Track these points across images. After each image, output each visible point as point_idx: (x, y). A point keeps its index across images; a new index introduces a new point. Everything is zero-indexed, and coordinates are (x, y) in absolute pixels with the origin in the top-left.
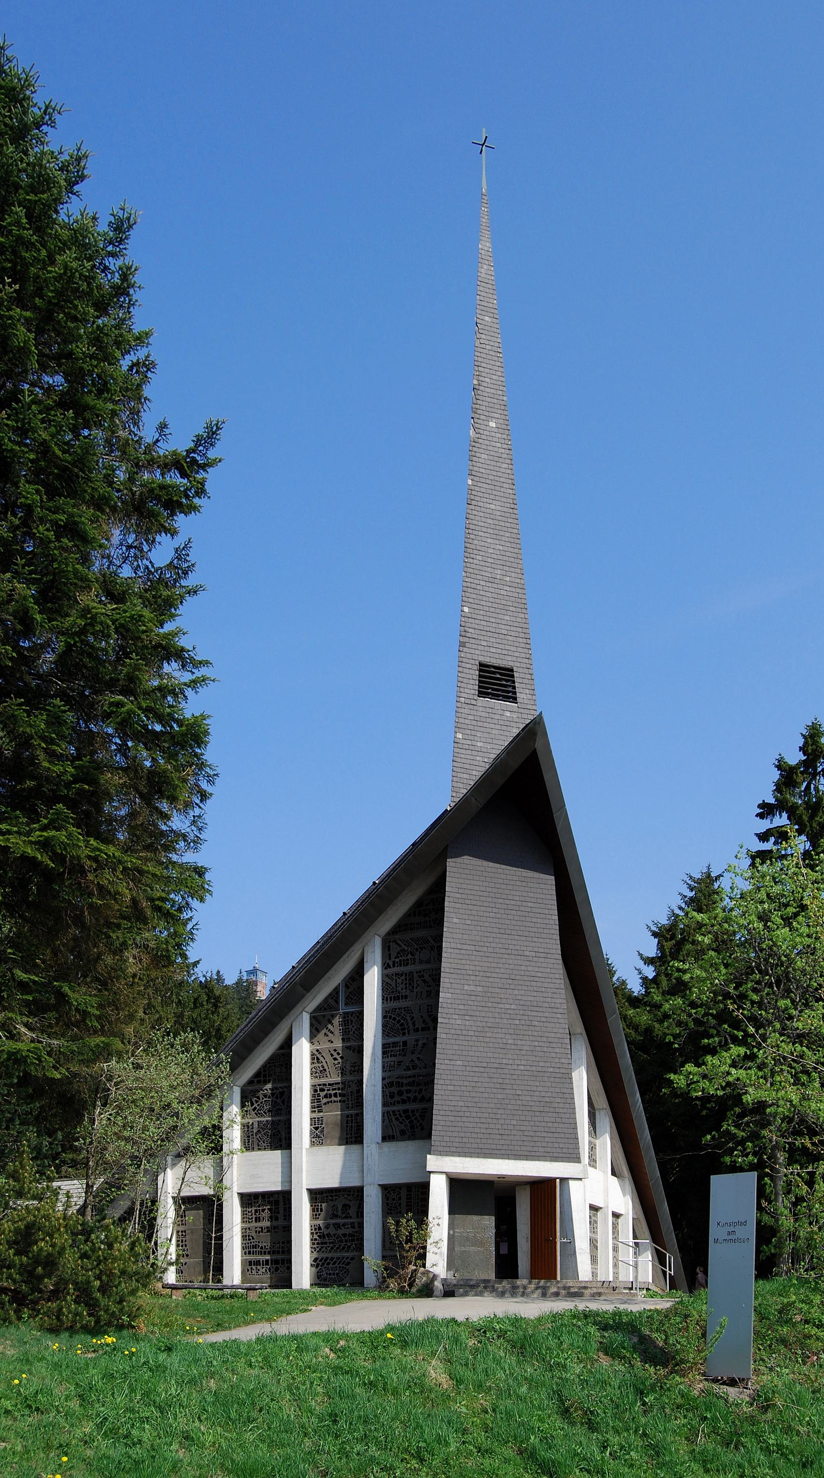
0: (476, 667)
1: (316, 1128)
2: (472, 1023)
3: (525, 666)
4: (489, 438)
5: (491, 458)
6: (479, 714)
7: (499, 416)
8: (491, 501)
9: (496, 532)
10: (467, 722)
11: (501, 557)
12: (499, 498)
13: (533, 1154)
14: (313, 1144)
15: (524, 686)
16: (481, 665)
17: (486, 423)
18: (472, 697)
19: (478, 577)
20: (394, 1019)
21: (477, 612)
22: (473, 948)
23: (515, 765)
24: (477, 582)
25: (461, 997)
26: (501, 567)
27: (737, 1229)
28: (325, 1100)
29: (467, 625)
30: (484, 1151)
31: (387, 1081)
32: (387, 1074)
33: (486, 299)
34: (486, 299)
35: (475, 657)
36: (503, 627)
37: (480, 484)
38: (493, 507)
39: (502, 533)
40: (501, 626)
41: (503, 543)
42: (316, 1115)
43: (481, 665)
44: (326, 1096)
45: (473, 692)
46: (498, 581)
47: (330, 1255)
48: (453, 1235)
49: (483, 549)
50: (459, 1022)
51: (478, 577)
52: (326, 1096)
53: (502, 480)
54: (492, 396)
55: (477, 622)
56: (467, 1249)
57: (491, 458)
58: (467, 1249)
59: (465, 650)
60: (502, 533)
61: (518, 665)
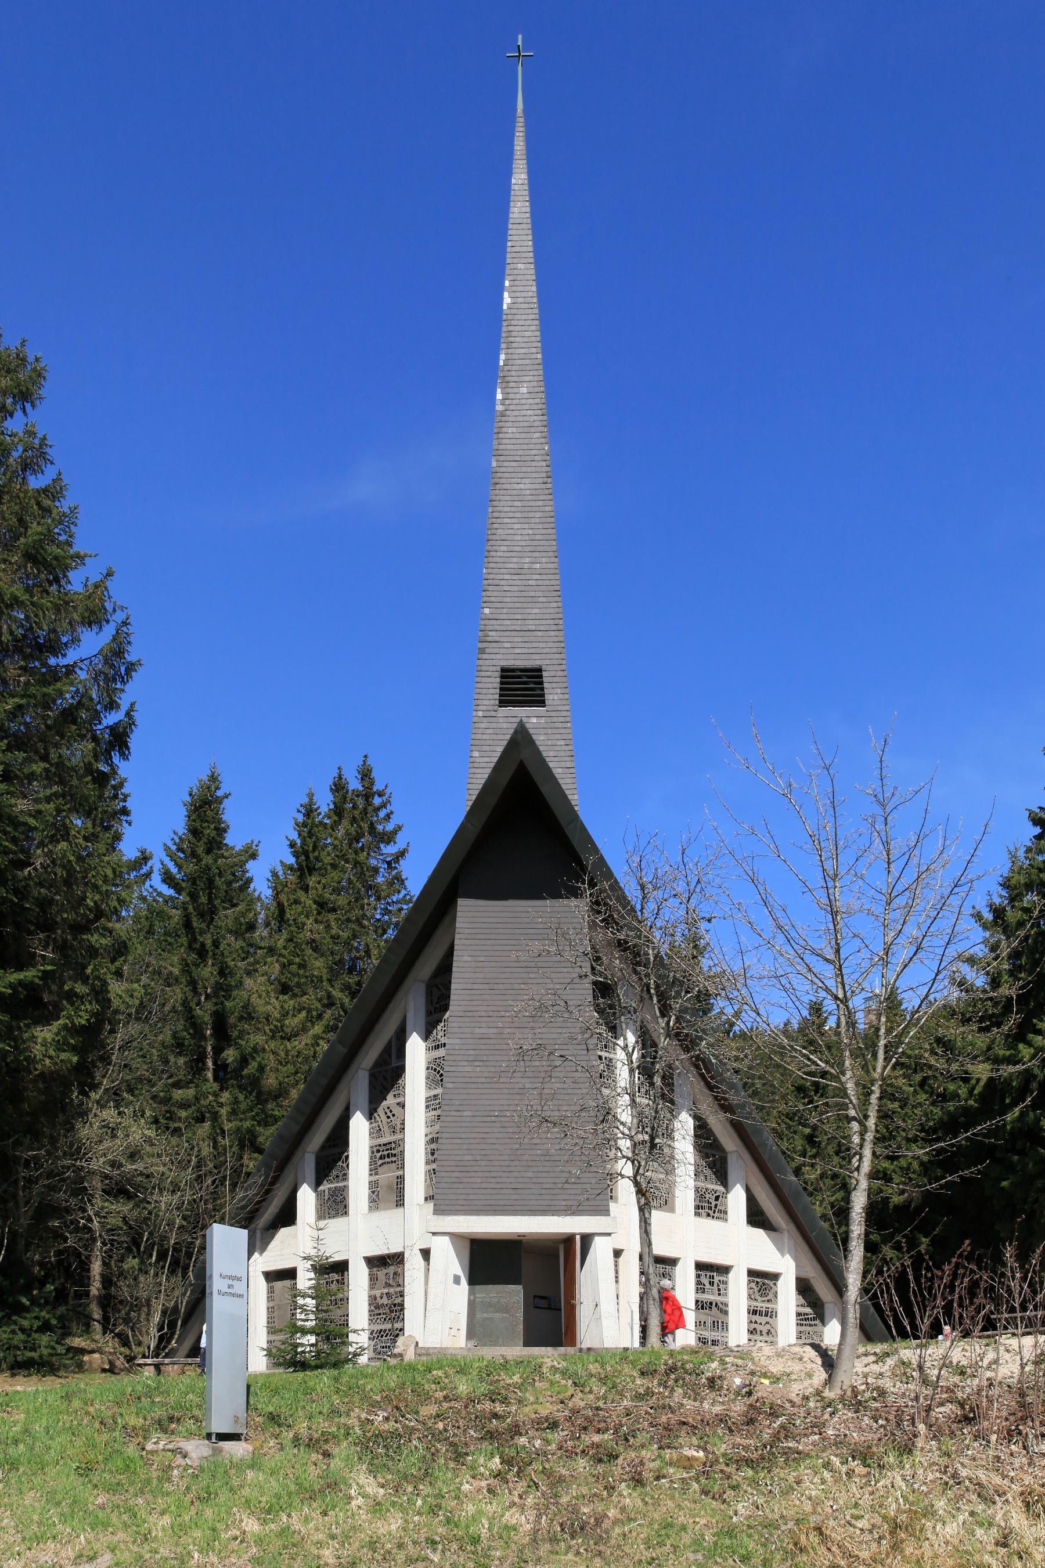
0: (498, 674)
1: (373, 1192)
2: (484, 1069)
3: (556, 662)
4: (519, 407)
5: (521, 430)
6: (500, 725)
7: (531, 378)
8: (519, 481)
9: (525, 515)
10: (485, 737)
11: (530, 543)
12: (529, 475)
13: (553, 1208)
14: (370, 1209)
15: (554, 685)
16: (503, 670)
17: (515, 390)
18: (491, 708)
19: (502, 571)
20: (435, 1070)
21: (499, 611)
22: (486, 986)
23: (504, 780)
24: (501, 577)
25: (471, 1041)
26: (530, 554)
27: (235, 1283)
28: (381, 1162)
29: (488, 628)
30: (553, 1208)
31: (430, 1137)
32: (430, 1129)
33: (518, 244)
34: (518, 244)
35: (494, 662)
36: (531, 622)
37: (506, 464)
38: (522, 486)
39: (531, 515)
40: (528, 622)
41: (533, 526)
42: (374, 1178)
43: (503, 670)
44: (381, 1158)
45: (492, 702)
46: (526, 571)
47: (383, 1327)
48: (474, 1300)
49: (509, 538)
50: (467, 1069)
51: (502, 571)
52: (381, 1158)
53: (533, 452)
54: (523, 356)
55: (499, 622)
56: (490, 1315)
57: (521, 430)
58: (490, 1315)
59: (485, 656)
60: (531, 515)
61: (548, 662)
